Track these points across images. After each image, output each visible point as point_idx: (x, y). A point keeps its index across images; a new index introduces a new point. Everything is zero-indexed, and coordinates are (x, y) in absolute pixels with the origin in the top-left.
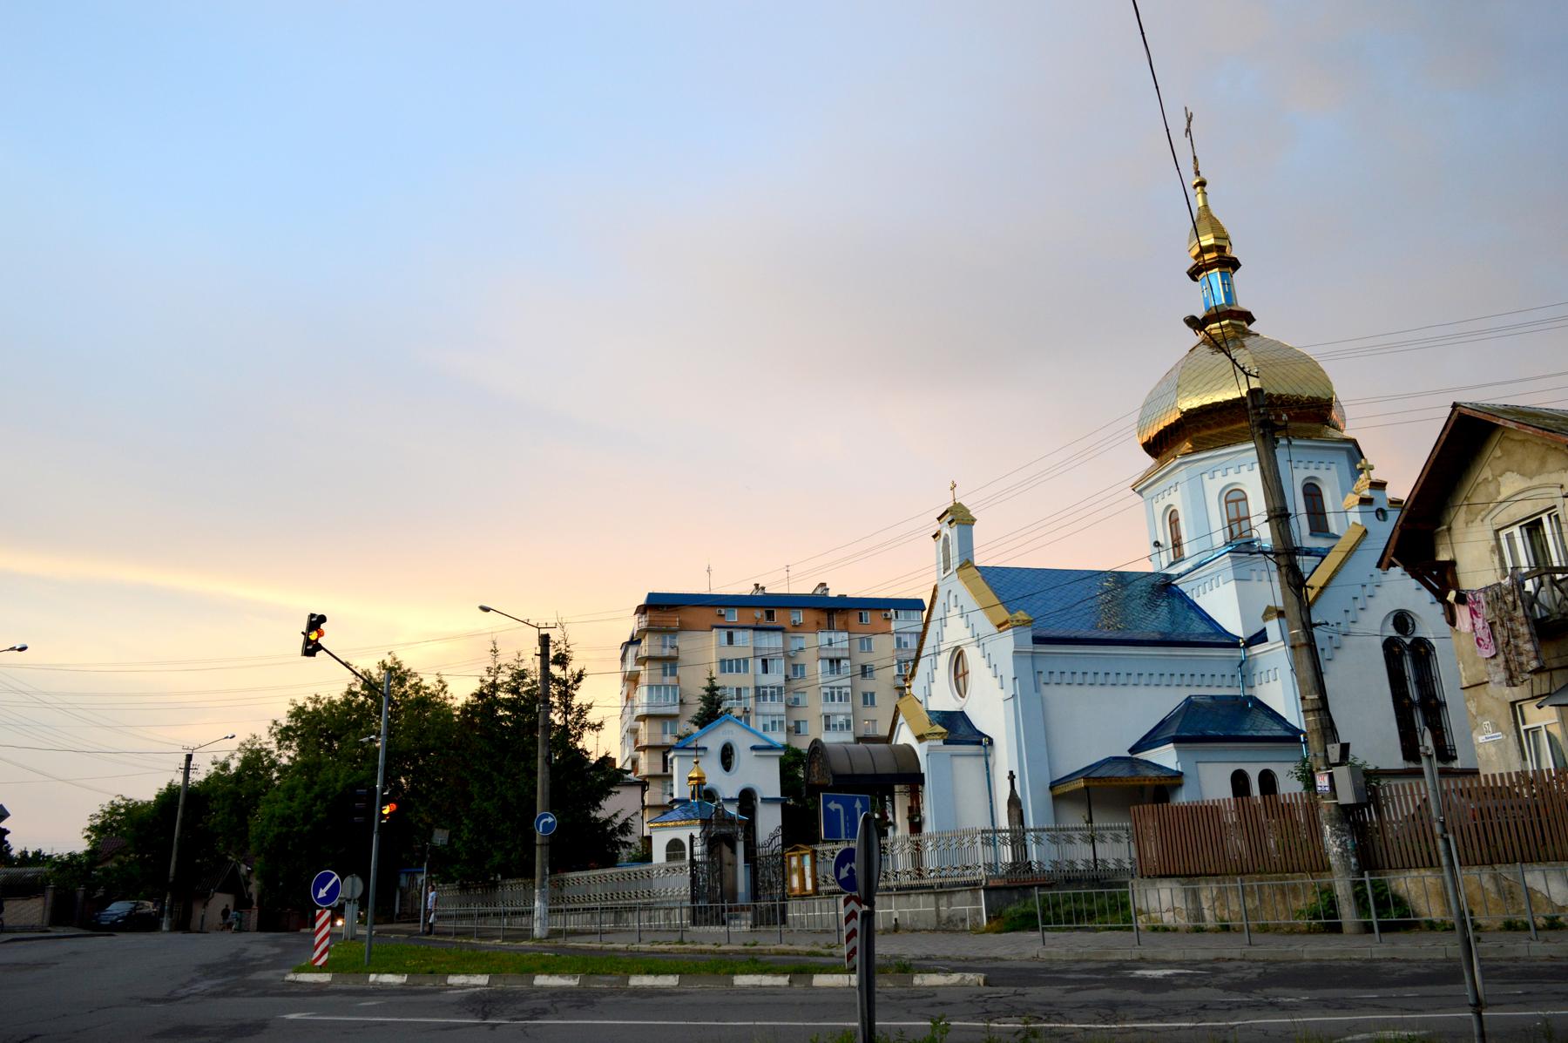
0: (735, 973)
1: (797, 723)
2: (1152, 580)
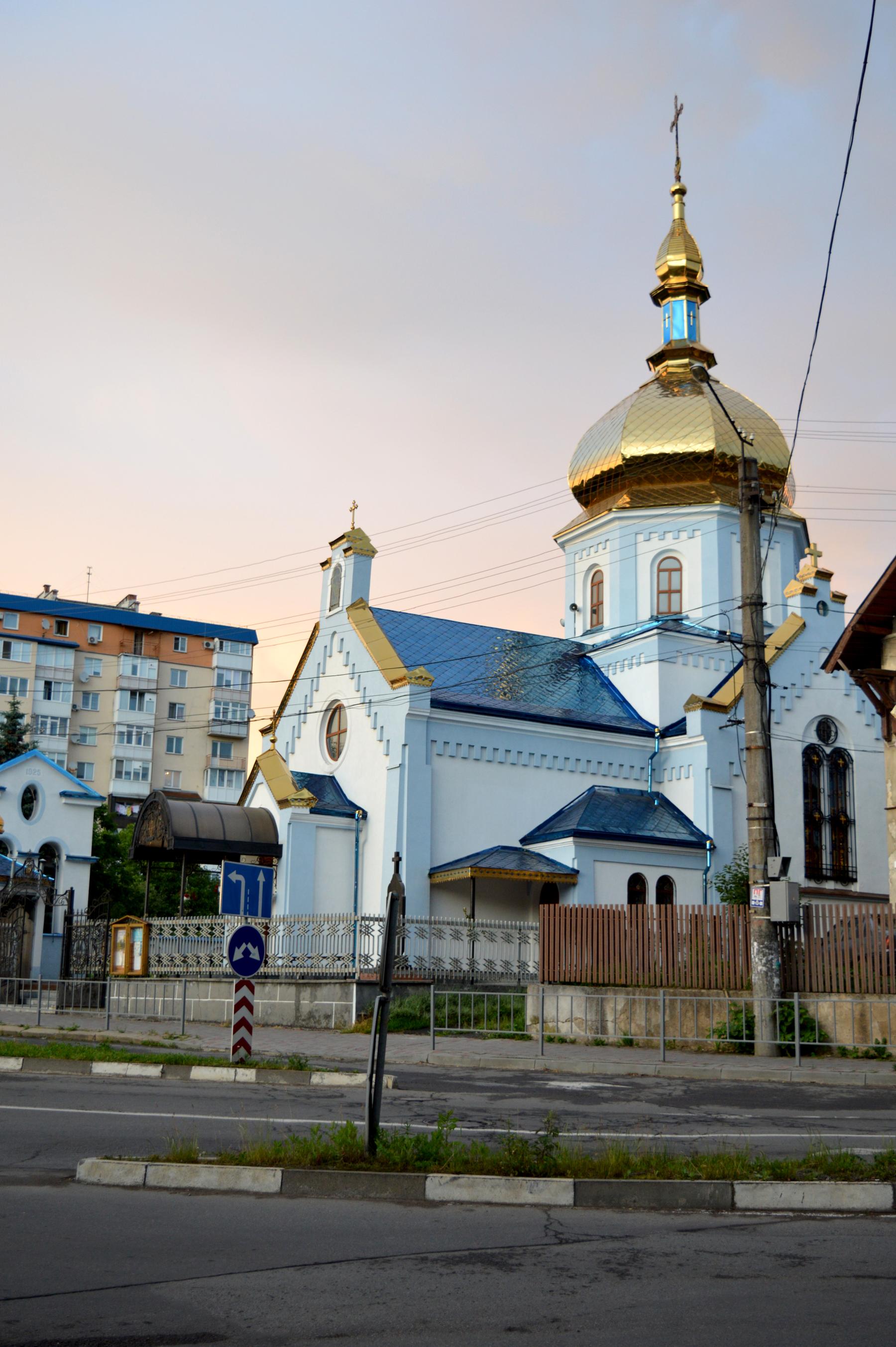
0: (92, 1060)
1: (81, 765)
2: (561, 647)
